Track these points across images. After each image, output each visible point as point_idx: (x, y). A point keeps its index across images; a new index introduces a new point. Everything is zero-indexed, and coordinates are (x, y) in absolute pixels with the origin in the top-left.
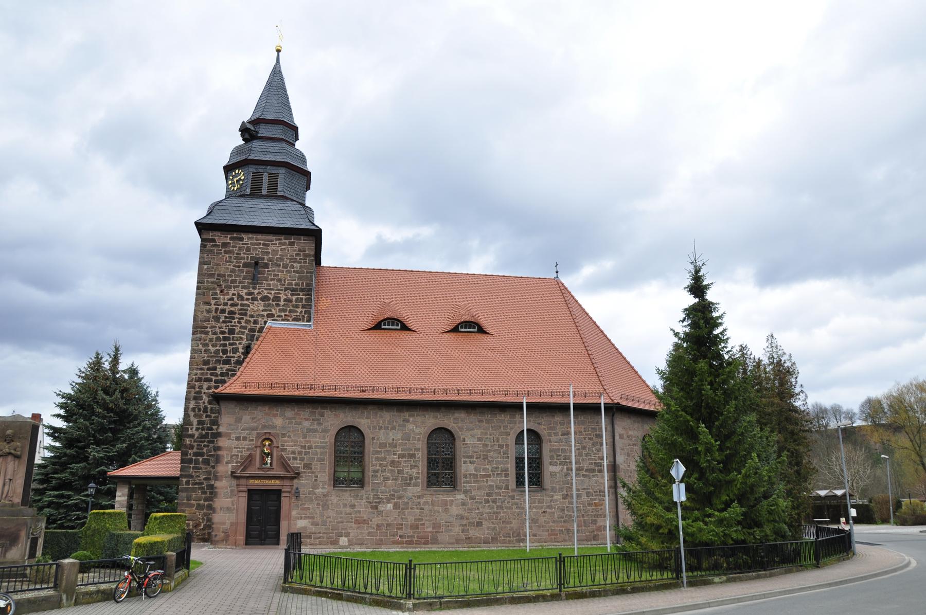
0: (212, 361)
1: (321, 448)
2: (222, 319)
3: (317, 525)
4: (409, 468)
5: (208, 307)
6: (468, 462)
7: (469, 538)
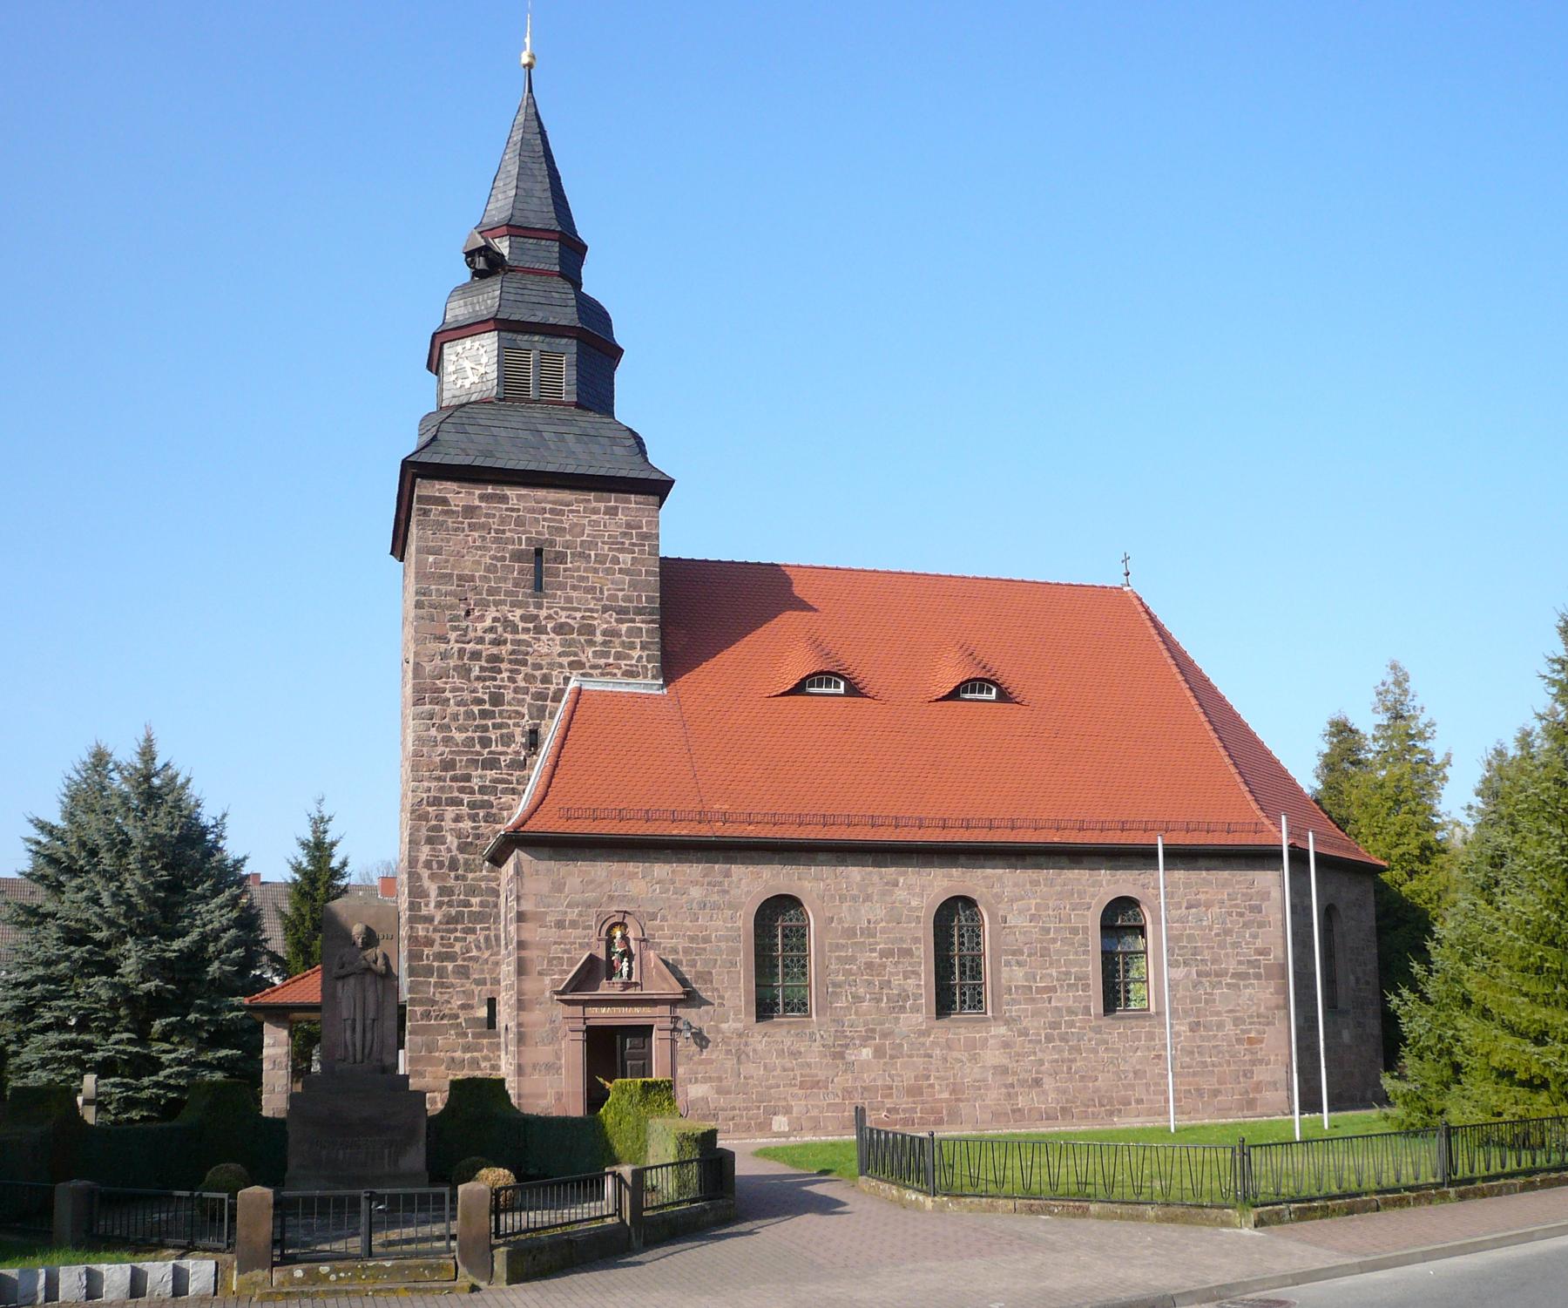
0: (461, 761)
1: (727, 941)
2: (476, 672)
3: (728, 1092)
4: (901, 976)
5: (443, 646)
6: (1013, 962)
7: (1019, 1110)
